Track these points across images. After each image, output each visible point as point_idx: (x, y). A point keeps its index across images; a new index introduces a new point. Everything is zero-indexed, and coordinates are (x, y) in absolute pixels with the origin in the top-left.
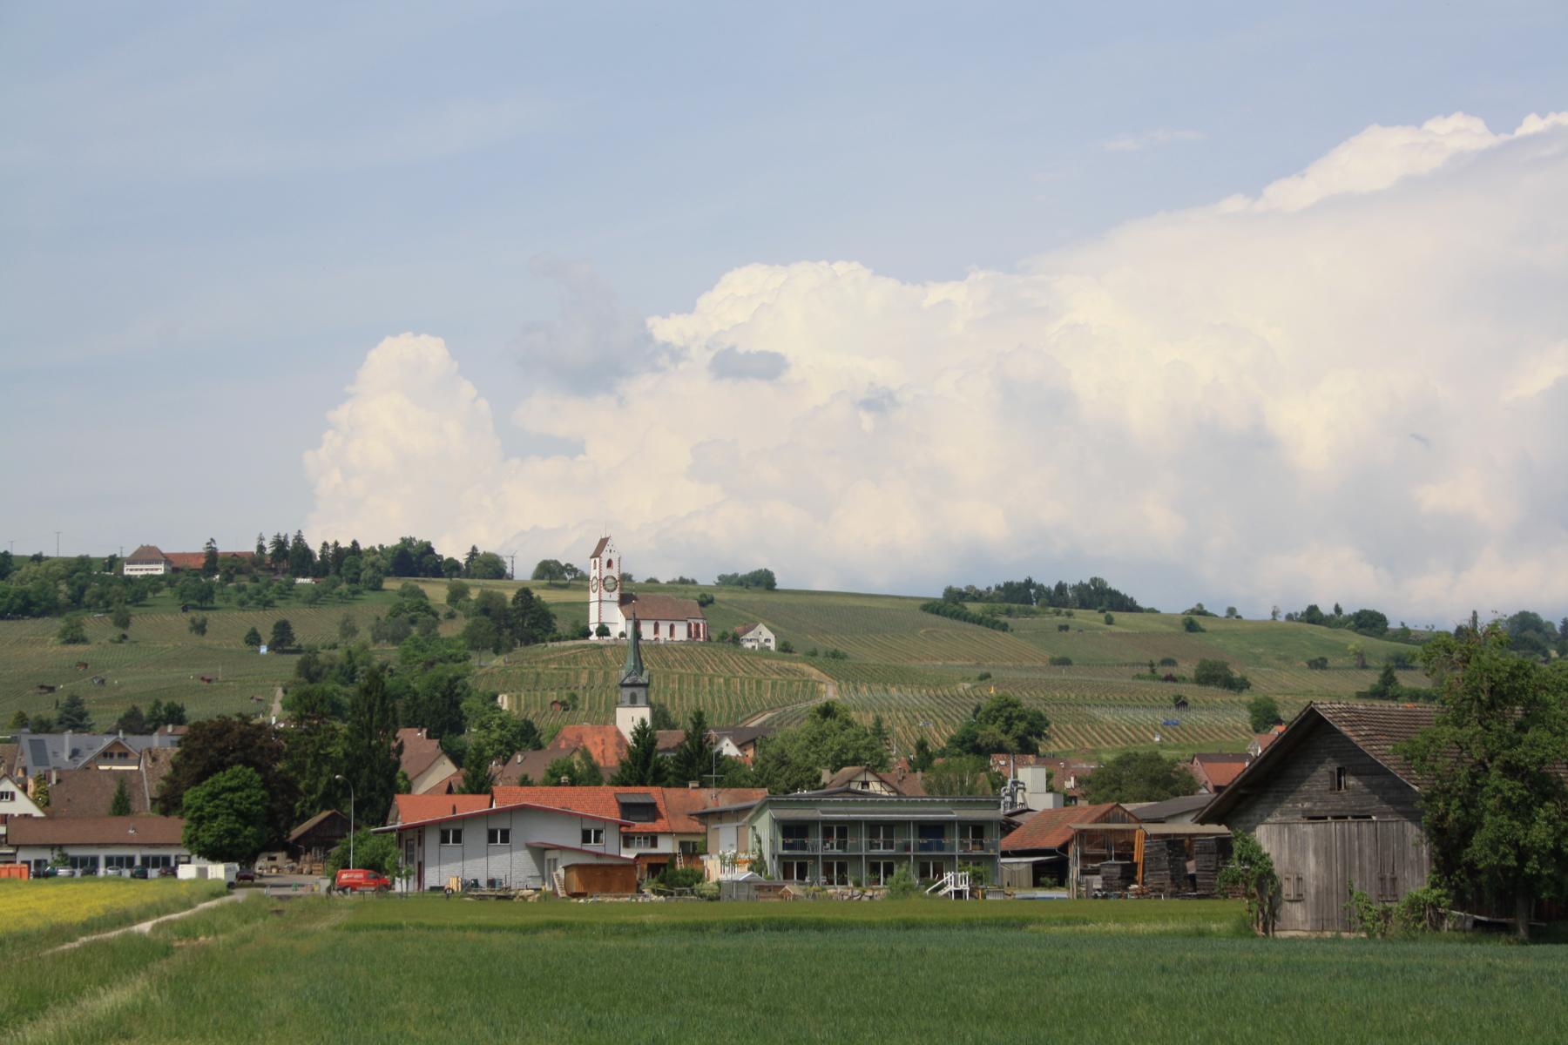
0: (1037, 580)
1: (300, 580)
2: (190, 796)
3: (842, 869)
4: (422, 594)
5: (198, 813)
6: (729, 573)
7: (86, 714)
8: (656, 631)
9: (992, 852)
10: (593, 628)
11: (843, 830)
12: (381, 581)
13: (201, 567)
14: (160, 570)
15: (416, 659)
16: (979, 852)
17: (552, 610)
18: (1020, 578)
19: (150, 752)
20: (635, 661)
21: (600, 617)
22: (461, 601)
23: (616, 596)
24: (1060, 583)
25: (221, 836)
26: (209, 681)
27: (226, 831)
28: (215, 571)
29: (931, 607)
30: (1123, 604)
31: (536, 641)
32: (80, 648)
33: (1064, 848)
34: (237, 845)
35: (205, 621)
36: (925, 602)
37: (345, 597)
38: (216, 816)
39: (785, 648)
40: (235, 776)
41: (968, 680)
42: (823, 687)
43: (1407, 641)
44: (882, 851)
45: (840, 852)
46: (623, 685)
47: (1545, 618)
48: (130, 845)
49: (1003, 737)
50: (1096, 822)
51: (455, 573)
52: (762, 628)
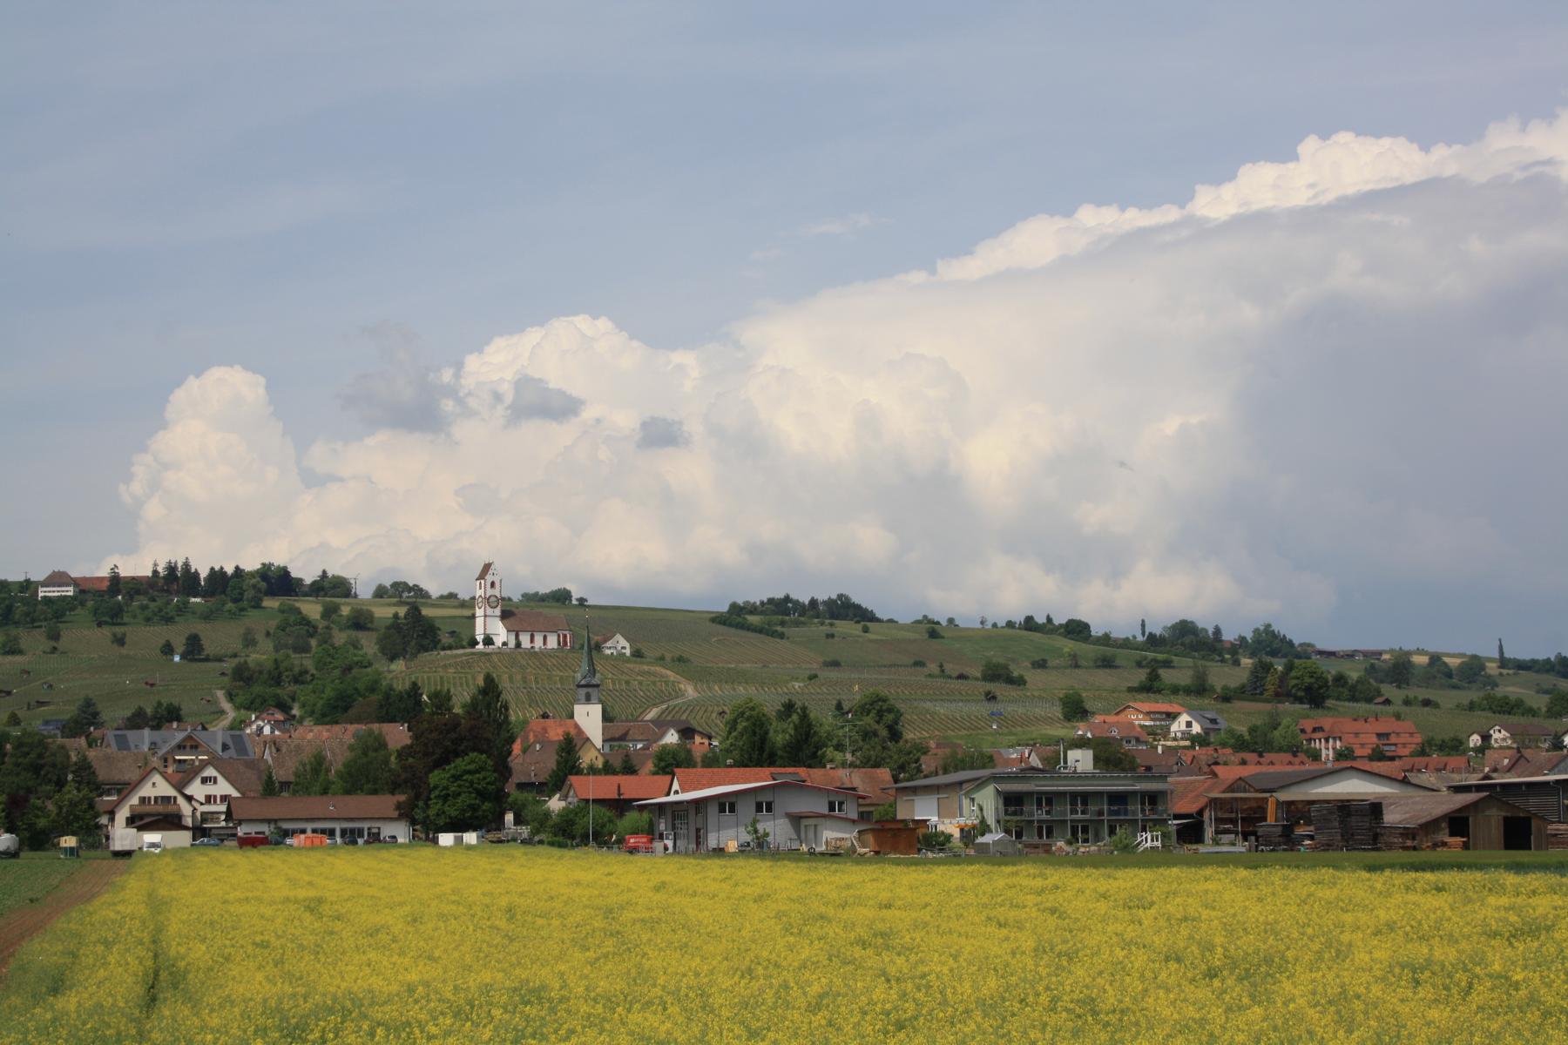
0: (794, 596)
1: (193, 600)
2: (436, 779)
3: (1085, 830)
4: (299, 612)
5: (444, 792)
6: (532, 591)
7: (97, 714)
8: (532, 641)
9: (1165, 816)
10: (480, 638)
11: (1049, 799)
12: (261, 600)
13: (105, 589)
14: (70, 591)
15: (332, 665)
16: (1155, 817)
17: (437, 624)
18: (780, 595)
19: (275, 744)
20: (589, 666)
21: (485, 629)
22: (334, 617)
23: (498, 611)
24: (813, 598)
25: (464, 810)
26: (152, 685)
27: (468, 806)
28: (118, 592)
29: (719, 619)
30: (863, 616)
31: (427, 651)
32: (18, 658)
33: (1200, 812)
34: (477, 817)
35: (124, 635)
36: (714, 615)
37: (234, 614)
38: (459, 794)
39: (637, 654)
40: (472, 762)
41: (797, 679)
42: (682, 686)
43: (1108, 645)
44: (1079, 816)
45: (1048, 817)
46: (579, 686)
47: (1200, 625)
48: (301, 819)
49: (877, 727)
50: (1224, 792)
51: (322, 593)
52: (619, 637)
